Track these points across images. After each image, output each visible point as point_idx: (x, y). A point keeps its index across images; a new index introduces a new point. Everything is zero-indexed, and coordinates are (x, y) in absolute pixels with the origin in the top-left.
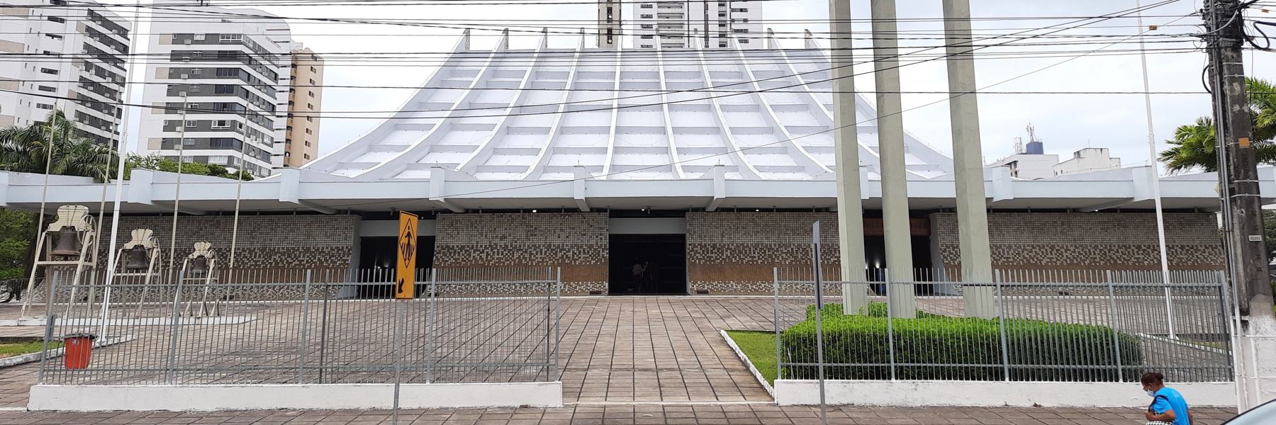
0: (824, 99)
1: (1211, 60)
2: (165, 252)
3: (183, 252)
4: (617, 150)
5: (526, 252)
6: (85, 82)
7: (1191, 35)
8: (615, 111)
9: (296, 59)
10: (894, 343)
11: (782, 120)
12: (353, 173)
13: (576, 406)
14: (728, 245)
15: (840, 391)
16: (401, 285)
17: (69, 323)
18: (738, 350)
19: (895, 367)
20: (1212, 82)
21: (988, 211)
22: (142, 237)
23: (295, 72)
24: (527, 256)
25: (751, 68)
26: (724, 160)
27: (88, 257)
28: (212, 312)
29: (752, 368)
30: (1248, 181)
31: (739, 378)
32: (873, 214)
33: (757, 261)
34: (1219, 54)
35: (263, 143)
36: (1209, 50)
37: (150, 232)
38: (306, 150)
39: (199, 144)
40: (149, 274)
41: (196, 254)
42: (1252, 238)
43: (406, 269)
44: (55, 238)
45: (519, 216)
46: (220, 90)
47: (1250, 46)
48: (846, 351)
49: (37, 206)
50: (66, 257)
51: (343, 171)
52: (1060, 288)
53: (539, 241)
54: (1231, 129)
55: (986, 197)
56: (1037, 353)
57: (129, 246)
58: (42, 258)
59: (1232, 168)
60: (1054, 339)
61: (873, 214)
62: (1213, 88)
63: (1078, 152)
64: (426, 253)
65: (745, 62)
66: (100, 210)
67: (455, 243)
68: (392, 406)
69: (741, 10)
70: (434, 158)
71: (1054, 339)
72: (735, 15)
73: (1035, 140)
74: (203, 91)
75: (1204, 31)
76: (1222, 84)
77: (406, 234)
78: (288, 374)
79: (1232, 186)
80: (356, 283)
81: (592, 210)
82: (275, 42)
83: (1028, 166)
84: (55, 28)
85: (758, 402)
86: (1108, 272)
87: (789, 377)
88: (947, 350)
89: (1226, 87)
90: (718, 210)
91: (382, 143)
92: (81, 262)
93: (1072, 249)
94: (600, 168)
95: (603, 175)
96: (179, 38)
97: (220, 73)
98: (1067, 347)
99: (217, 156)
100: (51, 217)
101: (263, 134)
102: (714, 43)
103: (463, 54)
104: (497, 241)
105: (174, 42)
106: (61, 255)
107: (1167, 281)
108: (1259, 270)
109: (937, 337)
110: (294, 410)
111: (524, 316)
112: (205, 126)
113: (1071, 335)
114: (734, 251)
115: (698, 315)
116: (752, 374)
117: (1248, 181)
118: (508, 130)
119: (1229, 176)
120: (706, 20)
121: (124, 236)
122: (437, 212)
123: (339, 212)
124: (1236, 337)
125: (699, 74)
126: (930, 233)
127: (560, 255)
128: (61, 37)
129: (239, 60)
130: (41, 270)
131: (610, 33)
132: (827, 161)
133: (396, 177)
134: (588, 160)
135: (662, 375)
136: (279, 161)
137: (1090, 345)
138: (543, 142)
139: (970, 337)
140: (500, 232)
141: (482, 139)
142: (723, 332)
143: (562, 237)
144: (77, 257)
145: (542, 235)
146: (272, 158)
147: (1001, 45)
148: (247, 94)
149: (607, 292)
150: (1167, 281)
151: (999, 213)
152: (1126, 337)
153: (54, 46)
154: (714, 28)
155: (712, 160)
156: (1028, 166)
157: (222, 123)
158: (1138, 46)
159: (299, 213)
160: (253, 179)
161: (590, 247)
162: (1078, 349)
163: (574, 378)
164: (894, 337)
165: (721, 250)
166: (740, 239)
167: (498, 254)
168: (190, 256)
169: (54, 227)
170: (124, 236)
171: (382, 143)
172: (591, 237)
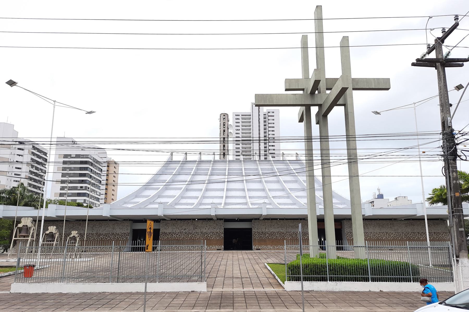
0: (303, 178)
1: (445, 164)
2: (61, 234)
3: (67, 235)
4: (227, 197)
5: (193, 234)
6: (31, 172)
7: (438, 155)
9: (109, 164)
11: (287, 186)
12: (130, 206)
14: (268, 232)
15: (309, 286)
16: (147, 247)
17: (25, 261)
18: (271, 271)
19: (329, 277)
20: (445, 172)
21: (363, 219)
22: (52, 229)
24: (194, 236)
25: (276, 167)
26: (266, 201)
27: (33, 237)
28: (78, 257)
29: (277, 277)
30: (459, 208)
31: (271, 281)
32: (321, 221)
33: (278, 238)
35: (97, 194)
36: (444, 160)
37: (55, 227)
38: (113, 197)
39: (73, 195)
40: (55, 243)
41: (72, 235)
42: (460, 229)
43: (149, 241)
44: (20, 229)
45: (191, 221)
46: (81, 175)
47: (460, 159)
48: (311, 271)
50: (24, 237)
53: (198, 230)
54: (452, 190)
55: (363, 214)
56: (381, 272)
58: (16, 237)
60: (387, 267)
61: (321, 221)
62: (446, 174)
63: (396, 198)
64: (156, 235)
67: (168, 231)
68: (144, 291)
69: (273, 146)
70: (160, 200)
71: (387, 267)
72: (270, 148)
73: (380, 194)
74: (75, 175)
75: (442, 153)
76: (449, 173)
77: (149, 228)
78: (106, 279)
80: (131, 246)
81: (218, 219)
82: (101, 158)
83: (378, 203)
84: (20, 152)
85: (279, 290)
87: (290, 280)
89: (451, 174)
92: (30, 238)
94: (221, 204)
96: (66, 156)
97: (81, 169)
98: (392, 270)
99: (80, 199)
100: (19, 222)
101: (97, 191)
102: (262, 158)
103: (170, 162)
104: (183, 230)
105: (64, 158)
107: (429, 245)
108: (463, 241)
109: (344, 266)
110: (108, 293)
114: (270, 234)
116: (276, 279)
118: (187, 190)
119: (452, 207)
120: (260, 149)
121: (46, 229)
122: (160, 220)
124: (454, 266)
125: (257, 169)
126: (342, 228)
127: (206, 236)
128: (22, 156)
130: (15, 241)
131: (224, 154)
132: (304, 201)
135: (243, 280)
136: (103, 201)
137: (401, 269)
138: (199, 194)
140: (184, 227)
142: (266, 264)
144: (28, 236)
145: (199, 228)
146: (100, 200)
147: (368, 158)
150: (429, 245)
151: (367, 220)
152: (414, 266)
153: (20, 159)
154: (262, 152)
155: (262, 201)
156: (378, 203)
157: (81, 187)
158: (418, 159)
159: (110, 220)
162: (396, 270)
163: (211, 281)
164: (328, 266)
165: (265, 234)
166: (272, 230)
167: (183, 235)
168: (70, 236)
169: (20, 225)
170: (46, 229)
172: (217, 229)
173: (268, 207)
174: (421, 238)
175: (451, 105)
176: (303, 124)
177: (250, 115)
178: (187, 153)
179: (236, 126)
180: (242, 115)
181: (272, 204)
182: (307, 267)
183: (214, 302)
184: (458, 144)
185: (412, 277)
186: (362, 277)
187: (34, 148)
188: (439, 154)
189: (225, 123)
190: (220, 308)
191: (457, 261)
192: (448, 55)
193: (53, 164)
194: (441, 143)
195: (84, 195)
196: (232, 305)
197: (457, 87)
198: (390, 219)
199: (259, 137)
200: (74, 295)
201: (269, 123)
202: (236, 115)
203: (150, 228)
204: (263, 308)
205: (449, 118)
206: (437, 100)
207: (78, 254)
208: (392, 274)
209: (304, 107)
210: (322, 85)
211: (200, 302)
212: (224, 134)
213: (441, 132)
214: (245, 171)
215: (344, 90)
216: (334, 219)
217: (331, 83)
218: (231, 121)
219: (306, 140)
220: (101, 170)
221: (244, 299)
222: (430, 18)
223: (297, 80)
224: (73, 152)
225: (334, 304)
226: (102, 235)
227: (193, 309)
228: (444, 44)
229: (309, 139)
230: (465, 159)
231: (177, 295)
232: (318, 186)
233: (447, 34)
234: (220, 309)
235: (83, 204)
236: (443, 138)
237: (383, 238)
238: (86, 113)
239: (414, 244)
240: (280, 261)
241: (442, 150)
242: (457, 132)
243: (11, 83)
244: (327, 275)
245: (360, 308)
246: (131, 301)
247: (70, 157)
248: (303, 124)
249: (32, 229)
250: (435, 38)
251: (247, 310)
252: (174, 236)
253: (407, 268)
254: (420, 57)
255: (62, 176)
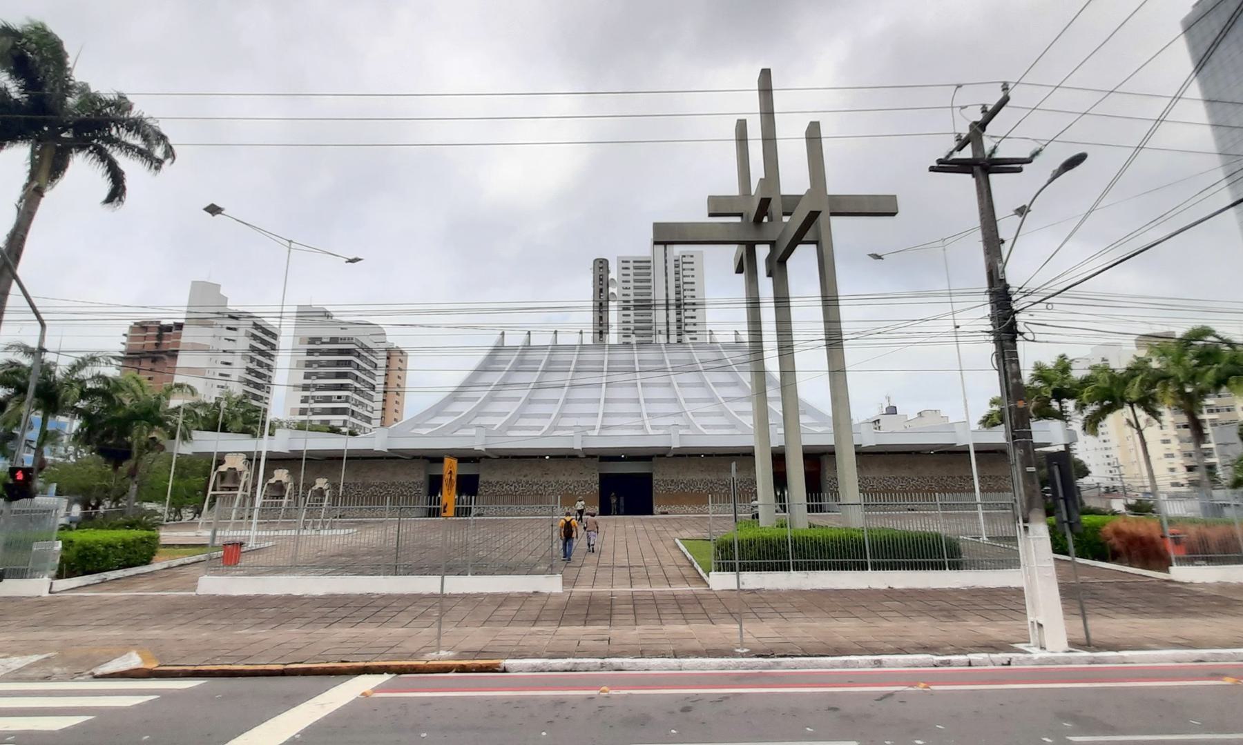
0: (746, 378)
1: (997, 348)
2: (296, 485)
3: (308, 486)
4: (605, 415)
5: (541, 485)
6: (250, 371)
7: (983, 332)
8: (566, 388)
9: (390, 353)
10: (792, 546)
11: (719, 393)
12: (425, 431)
13: (571, 592)
15: (752, 580)
16: (445, 507)
17: (229, 534)
19: (793, 562)
20: (998, 364)
21: (857, 453)
22: (281, 475)
23: (389, 362)
25: (697, 356)
26: (679, 421)
27: (245, 489)
28: (327, 527)
29: (696, 565)
30: (1024, 430)
31: (686, 571)
32: (779, 458)
34: (1001, 344)
35: (367, 411)
36: (995, 341)
37: (286, 471)
38: (396, 416)
39: (324, 412)
40: (285, 501)
41: (317, 487)
42: (1029, 469)
43: (448, 496)
44: (223, 476)
47: (1022, 339)
48: (759, 551)
49: (211, 454)
50: (230, 489)
51: (417, 430)
52: (909, 506)
53: (551, 479)
54: (1011, 395)
55: (855, 443)
56: (890, 551)
57: (272, 481)
58: (214, 489)
59: (1013, 421)
60: (901, 541)
61: (779, 458)
62: (999, 367)
63: (920, 413)
64: (468, 486)
65: (693, 351)
66: (343, 455)
67: (493, 479)
68: (439, 592)
69: (692, 317)
70: (477, 421)
71: (901, 541)
72: (688, 321)
73: (891, 405)
74: (328, 376)
75: (991, 328)
76: (1004, 365)
77: (449, 472)
78: (375, 570)
79: (1014, 434)
80: (428, 506)
81: (588, 456)
83: (888, 423)
84: (231, 334)
85: (699, 589)
86: (937, 494)
87: (719, 570)
88: (828, 550)
89: (1007, 366)
90: (675, 456)
91: (444, 411)
92: (240, 493)
93: (916, 479)
94: (593, 428)
95: (596, 433)
96: (313, 341)
97: (339, 363)
98: (910, 547)
99: (336, 420)
100: (221, 462)
101: (367, 405)
102: (673, 339)
103: (498, 349)
104: (521, 478)
105: (309, 343)
106: (227, 487)
107: (978, 500)
108: (1034, 491)
109: (821, 541)
110: (378, 594)
111: (539, 530)
112: (328, 399)
113: (913, 538)
114: (687, 484)
115: (661, 529)
117: (1024, 430)
118: (530, 401)
119: (1011, 428)
120: (668, 323)
121: (268, 474)
122: (481, 458)
123: (415, 458)
124: (1020, 538)
125: (663, 361)
126: (820, 470)
127: (565, 488)
128: (233, 340)
129: (352, 355)
130: (214, 498)
131: (601, 333)
132: (749, 421)
133: (455, 434)
134: (583, 422)
135: (632, 570)
136: (376, 423)
137: (926, 545)
138: (554, 410)
139: (844, 540)
141: (512, 408)
142: (677, 541)
143: (568, 477)
144: (237, 488)
146: (373, 421)
147: (856, 339)
148: (356, 378)
149: (598, 513)
150: (978, 500)
151: (865, 456)
152: (950, 539)
153: (229, 346)
154: (673, 328)
155: (670, 421)
156: (888, 423)
157: (339, 397)
158: (954, 339)
159: (388, 458)
160: (357, 435)
161: (586, 482)
162: (918, 547)
163: (571, 572)
164: (792, 541)
165: (677, 484)
168: (313, 488)
169: (223, 468)
170: (268, 474)
171: (444, 411)
173: (681, 432)
174: (966, 488)
175: (1003, 242)
176: (742, 277)
177: (649, 262)
178: (558, 330)
179: (623, 282)
180: (635, 262)
181: (691, 427)
182: (751, 545)
183: (574, 612)
184: (1017, 312)
185: (946, 560)
186: (854, 562)
187: (256, 326)
188: (985, 330)
189: (602, 275)
190: (585, 623)
191: (1026, 528)
192: (993, 151)
193: (290, 354)
194: (987, 310)
195: (343, 411)
196: (608, 618)
197: (1018, 210)
198: (909, 453)
199: (667, 300)
200: (314, 599)
201: (684, 276)
202: (623, 262)
203: (451, 472)
204: (667, 623)
205: (1000, 265)
206: (978, 235)
207: (318, 522)
208: (911, 555)
209: (744, 246)
210: (775, 207)
211: (548, 613)
212: (600, 296)
213: (987, 289)
214: (639, 364)
215: (813, 216)
216: (804, 454)
217: (791, 203)
218: (613, 274)
219: (749, 305)
220: (374, 365)
221: (631, 606)
222: (959, 86)
223: (729, 199)
224: (326, 333)
225: (800, 613)
226: (373, 485)
227: (533, 626)
228: (985, 133)
229: (754, 305)
230: (1032, 339)
231: (503, 600)
232: (773, 392)
233: (990, 115)
234: (585, 625)
235: (341, 428)
236: (991, 300)
237: (897, 489)
238: (347, 262)
239: (950, 498)
240: (704, 534)
241: (990, 323)
242: (1015, 290)
243: (213, 210)
244: (789, 559)
245: (848, 621)
246: (418, 610)
247: (319, 342)
248: (742, 277)
249: (245, 474)
250: (969, 124)
251: (637, 627)
252: (505, 487)
253: (938, 544)
254: (943, 157)
255: (306, 378)
